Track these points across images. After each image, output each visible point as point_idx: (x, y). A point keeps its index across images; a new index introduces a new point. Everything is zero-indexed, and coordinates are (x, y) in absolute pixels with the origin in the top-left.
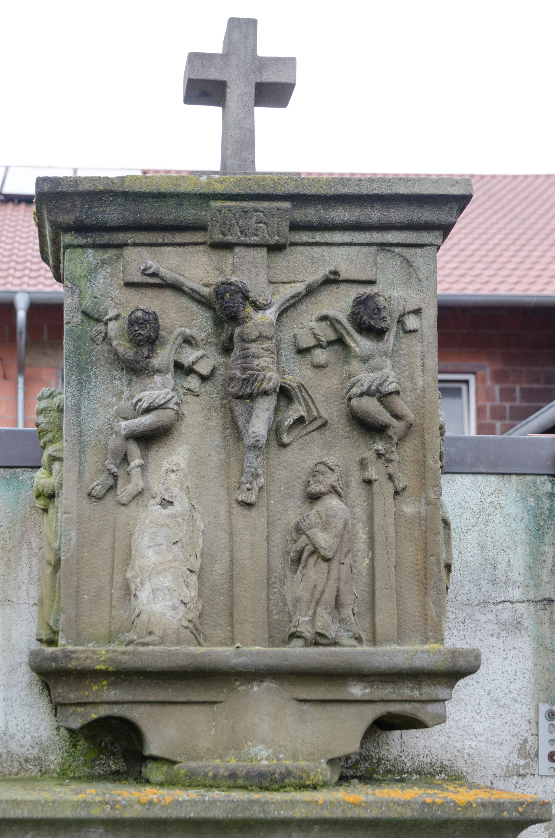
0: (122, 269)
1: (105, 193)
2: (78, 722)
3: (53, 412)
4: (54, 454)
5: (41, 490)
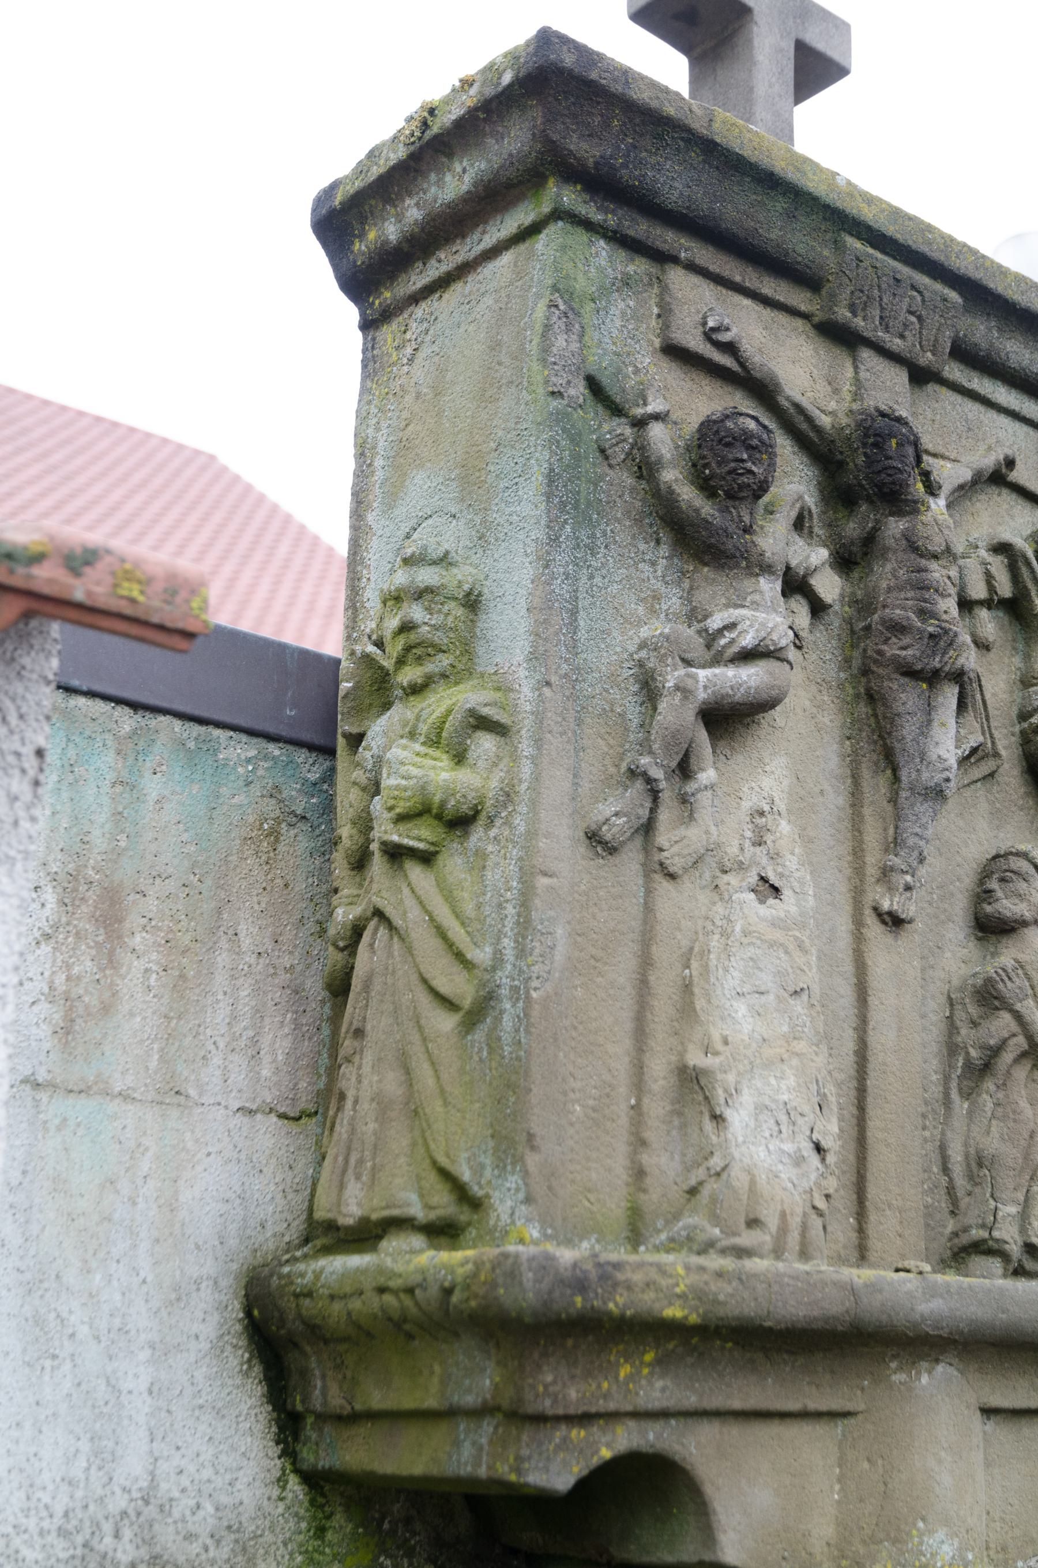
0: (656, 310)
1: (674, 127)
2: (571, 1472)
3: (453, 604)
4: (485, 711)
5: (437, 799)
